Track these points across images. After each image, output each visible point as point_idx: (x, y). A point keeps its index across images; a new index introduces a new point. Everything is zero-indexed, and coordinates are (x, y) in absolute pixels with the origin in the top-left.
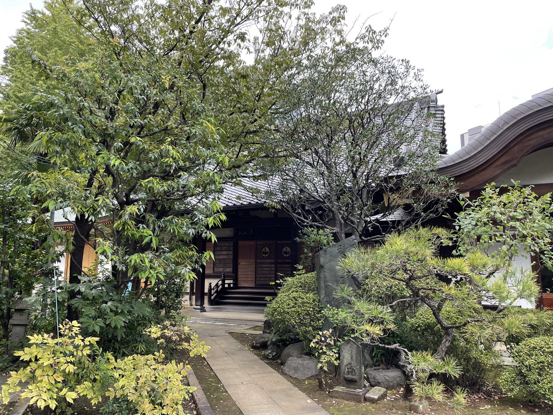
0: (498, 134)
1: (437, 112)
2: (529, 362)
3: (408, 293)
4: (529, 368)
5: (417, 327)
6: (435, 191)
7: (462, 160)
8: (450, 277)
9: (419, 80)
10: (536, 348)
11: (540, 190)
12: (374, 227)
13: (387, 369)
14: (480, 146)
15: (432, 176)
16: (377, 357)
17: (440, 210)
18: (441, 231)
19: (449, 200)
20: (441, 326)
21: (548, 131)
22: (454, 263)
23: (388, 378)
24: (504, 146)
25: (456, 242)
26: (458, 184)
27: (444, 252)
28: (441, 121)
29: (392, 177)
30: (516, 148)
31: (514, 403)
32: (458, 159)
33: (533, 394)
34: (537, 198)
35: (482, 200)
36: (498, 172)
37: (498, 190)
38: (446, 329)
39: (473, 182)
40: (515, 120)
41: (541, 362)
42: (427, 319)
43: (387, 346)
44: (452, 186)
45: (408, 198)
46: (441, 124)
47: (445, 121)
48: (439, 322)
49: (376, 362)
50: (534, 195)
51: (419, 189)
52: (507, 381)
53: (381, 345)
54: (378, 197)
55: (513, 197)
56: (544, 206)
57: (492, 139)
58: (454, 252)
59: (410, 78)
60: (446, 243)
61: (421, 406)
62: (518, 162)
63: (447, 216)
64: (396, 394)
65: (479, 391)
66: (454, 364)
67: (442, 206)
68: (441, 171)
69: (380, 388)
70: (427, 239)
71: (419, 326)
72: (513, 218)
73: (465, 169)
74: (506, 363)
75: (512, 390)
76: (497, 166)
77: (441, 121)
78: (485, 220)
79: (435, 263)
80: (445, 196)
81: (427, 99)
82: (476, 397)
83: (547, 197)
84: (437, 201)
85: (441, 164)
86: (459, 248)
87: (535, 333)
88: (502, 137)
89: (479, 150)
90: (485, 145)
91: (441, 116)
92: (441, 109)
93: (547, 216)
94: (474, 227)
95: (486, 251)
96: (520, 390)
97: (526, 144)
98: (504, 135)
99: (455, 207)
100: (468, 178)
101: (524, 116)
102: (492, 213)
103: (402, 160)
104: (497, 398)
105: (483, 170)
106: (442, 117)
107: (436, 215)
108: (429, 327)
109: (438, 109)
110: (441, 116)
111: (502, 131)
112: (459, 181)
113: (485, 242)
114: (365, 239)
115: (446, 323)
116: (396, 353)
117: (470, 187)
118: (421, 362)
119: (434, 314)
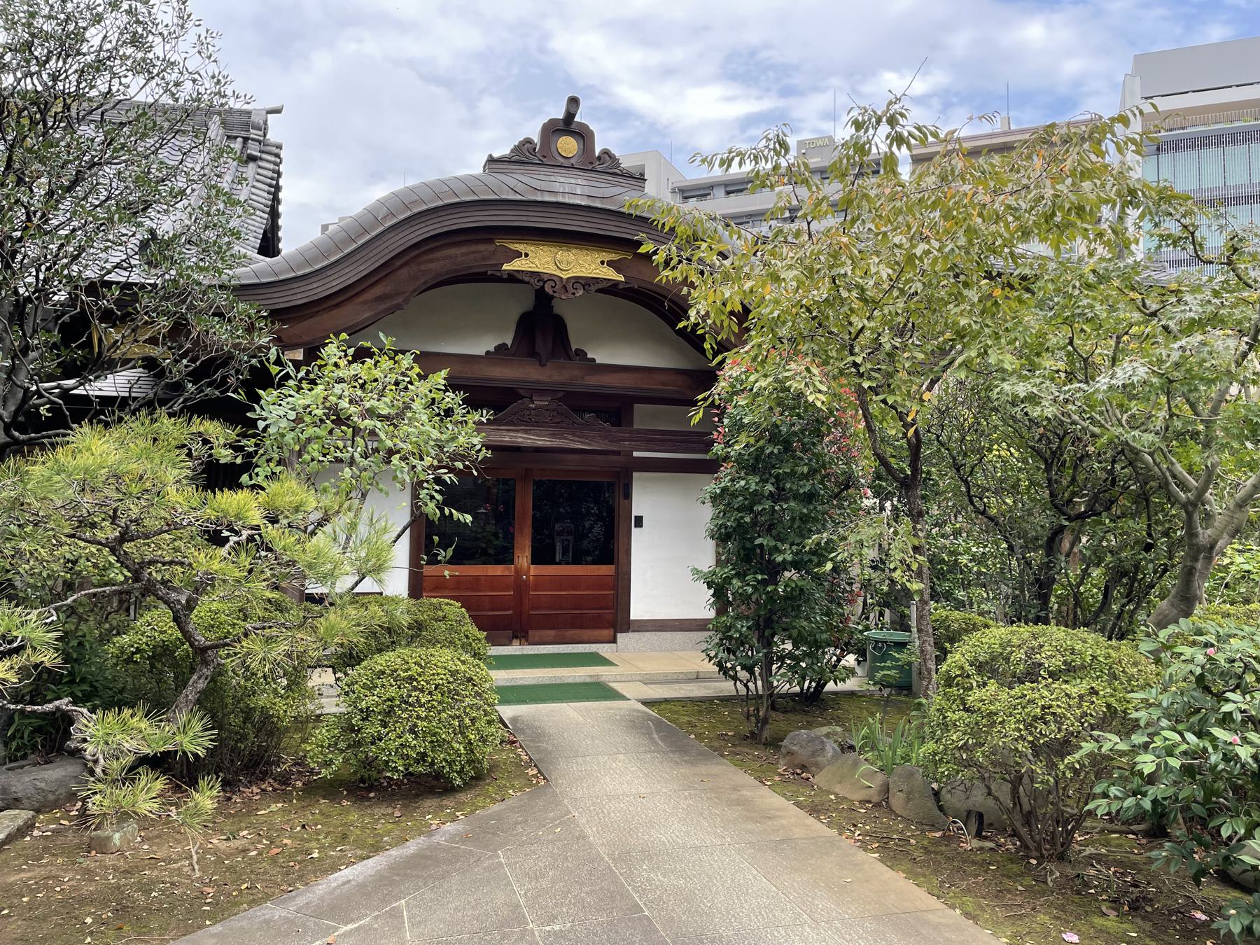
0: (374, 234)
1: (264, 156)
2: (368, 701)
3: (118, 575)
4: (366, 714)
5: (133, 653)
6: (222, 335)
7: (292, 275)
8: (226, 534)
9: (209, 58)
10: (383, 673)
11: (428, 362)
12: (54, 409)
13: (46, 763)
14: (335, 253)
15: (222, 299)
16: (22, 738)
17: (232, 380)
18: (213, 428)
19: (254, 361)
20: (192, 645)
21: (464, 249)
22: (228, 501)
23: (43, 785)
24: (382, 261)
25: (250, 455)
26: (277, 326)
27: (216, 476)
28: (272, 179)
29: (109, 285)
30: (405, 271)
31: (331, 789)
32: (287, 272)
33: (368, 763)
34: (423, 377)
35: (320, 367)
36: (366, 315)
37: (351, 351)
38: (203, 650)
39: (306, 328)
40: (409, 214)
41: (389, 700)
42: (162, 632)
43: (29, 708)
44: (261, 329)
45: (153, 341)
46: (270, 186)
47: (281, 182)
48: (188, 636)
49: (18, 749)
50: (417, 370)
51: (179, 328)
52: (322, 746)
53: (13, 707)
54: (74, 327)
55: (378, 370)
56: (433, 395)
57: (360, 242)
58: (245, 478)
59: (187, 42)
60: (225, 455)
61: (117, 835)
62: (406, 301)
63: (240, 396)
64: (60, 818)
65: (263, 777)
66: (198, 727)
67: (238, 372)
68: (244, 291)
69: (17, 811)
70: (174, 443)
71: (138, 650)
72: (370, 413)
73: (299, 297)
74: (326, 711)
75: (327, 764)
76: (365, 302)
77: (272, 179)
78: (319, 412)
79: (181, 497)
80: (244, 350)
81: (245, 119)
82: (256, 790)
83: (440, 378)
84: (226, 360)
85: (247, 275)
86: (257, 470)
87: (393, 642)
88: (378, 243)
89: (333, 259)
90: (346, 251)
91: (271, 166)
92: (275, 152)
93: (438, 415)
94: (293, 424)
95: (311, 480)
96: (346, 761)
97: (423, 267)
98: (384, 239)
99: (261, 379)
100: (304, 318)
101: (424, 207)
102: (333, 399)
103: (908, 484)
104: (299, 784)
105: (337, 306)
106: (274, 171)
107: (221, 393)
108: (162, 653)
109: (269, 148)
110: (271, 166)
111: (381, 229)
112: (283, 322)
113: (313, 460)
114: (22, 437)
115: (201, 639)
116: (67, 720)
117: (306, 339)
118: (105, 734)
119: (176, 619)
